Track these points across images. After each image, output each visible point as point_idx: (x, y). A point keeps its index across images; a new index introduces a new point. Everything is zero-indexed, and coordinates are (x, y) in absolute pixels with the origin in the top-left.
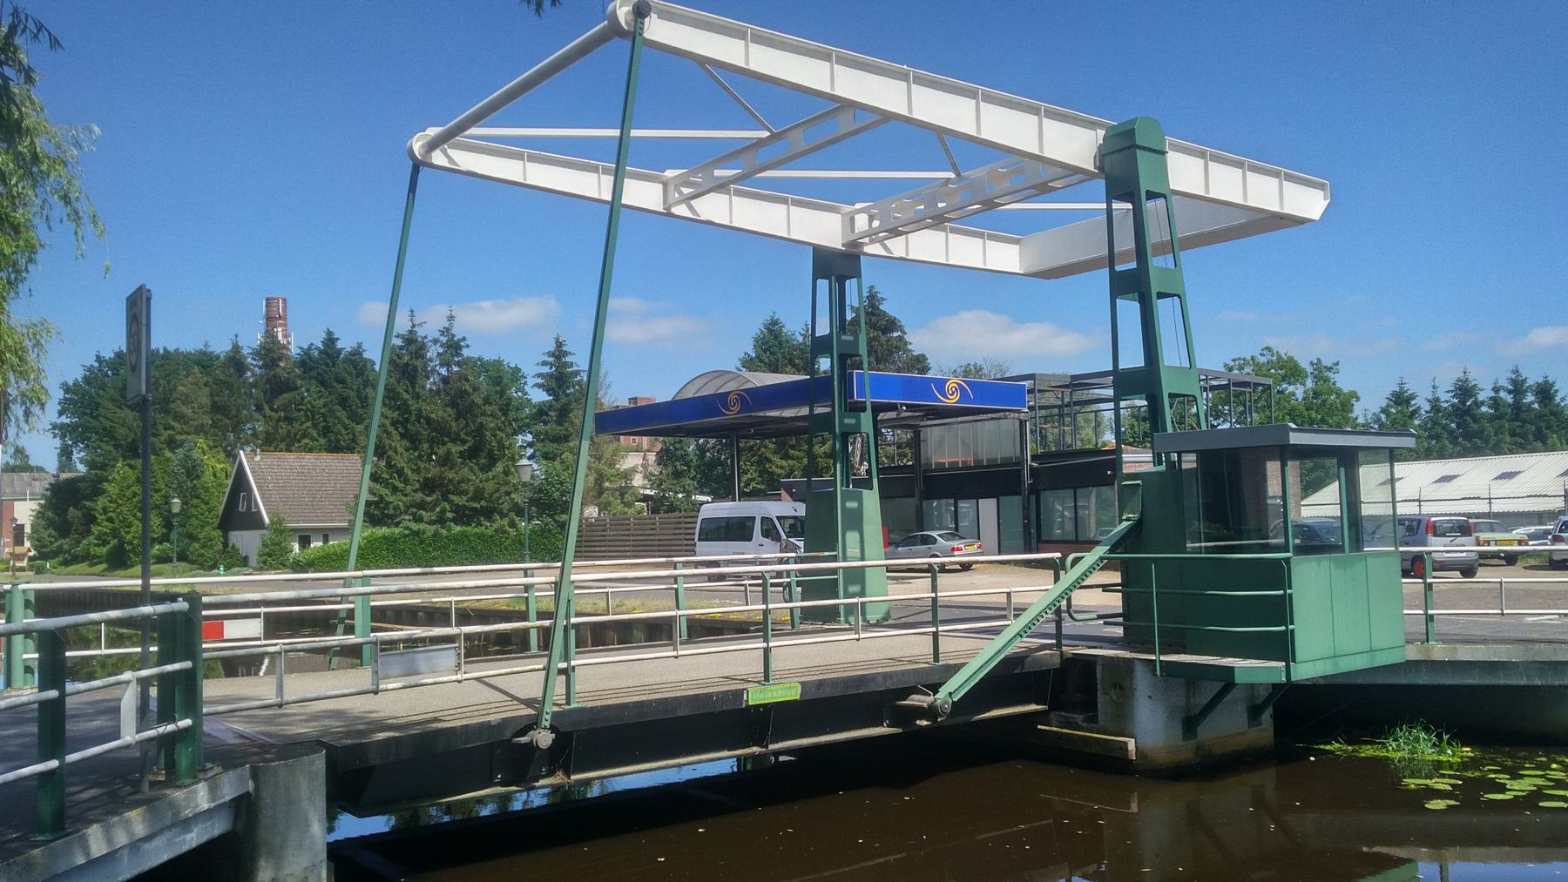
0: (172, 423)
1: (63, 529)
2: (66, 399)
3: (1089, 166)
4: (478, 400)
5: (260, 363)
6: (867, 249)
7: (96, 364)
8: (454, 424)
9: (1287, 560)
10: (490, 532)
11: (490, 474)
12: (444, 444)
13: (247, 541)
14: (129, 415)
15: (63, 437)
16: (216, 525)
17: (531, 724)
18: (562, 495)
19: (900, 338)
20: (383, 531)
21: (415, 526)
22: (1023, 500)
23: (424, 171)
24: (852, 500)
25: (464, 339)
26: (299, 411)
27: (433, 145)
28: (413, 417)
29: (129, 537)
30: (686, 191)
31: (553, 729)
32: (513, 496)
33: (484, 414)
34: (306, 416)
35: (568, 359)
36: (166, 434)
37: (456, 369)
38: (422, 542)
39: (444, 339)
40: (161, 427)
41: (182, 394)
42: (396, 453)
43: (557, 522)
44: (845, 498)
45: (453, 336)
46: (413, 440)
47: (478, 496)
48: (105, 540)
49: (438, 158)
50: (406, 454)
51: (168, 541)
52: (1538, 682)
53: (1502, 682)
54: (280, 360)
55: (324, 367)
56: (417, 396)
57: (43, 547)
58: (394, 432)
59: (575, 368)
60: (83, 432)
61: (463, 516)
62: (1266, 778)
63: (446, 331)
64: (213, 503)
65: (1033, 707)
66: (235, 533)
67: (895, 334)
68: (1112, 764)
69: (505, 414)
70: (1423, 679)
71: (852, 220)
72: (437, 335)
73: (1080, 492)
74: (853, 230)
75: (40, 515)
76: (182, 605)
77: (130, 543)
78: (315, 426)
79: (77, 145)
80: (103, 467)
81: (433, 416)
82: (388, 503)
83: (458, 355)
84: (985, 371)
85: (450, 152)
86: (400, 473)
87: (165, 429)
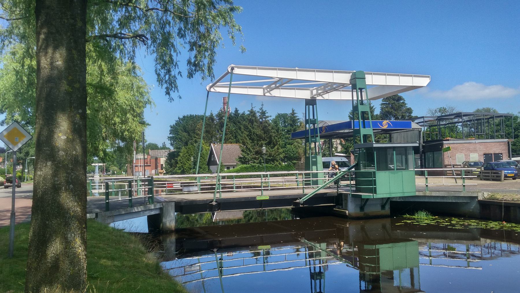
0: (196, 136)
1: (171, 165)
2: (171, 130)
3: (349, 83)
4: (270, 128)
5: (218, 118)
6: (317, 98)
7: (178, 120)
8: (263, 135)
9: (374, 172)
10: (274, 166)
11: (274, 149)
12: (261, 141)
13: (212, 168)
14: (185, 134)
15: (171, 140)
16: (206, 164)
17: (212, 201)
18: (294, 155)
19: (403, 103)
20: (245, 165)
21: (253, 164)
22: (420, 155)
23: (210, 93)
24: (314, 158)
25: (266, 111)
26: (228, 131)
27: (211, 87)
28: (252, 134)
29: (185, 167)
30: (268, 90)
31: (216, 202)
32: (280, 155)
33: (271, 132)
34: (230, 133)
35: (296, 115)
36: (194, 139)
37: (264, 119)
38: (255, 169)
39: (261, 111)
40: (193, 137)
41: (198, 128)
42: (248, 144)
43: (293, 163)
44: (313, 158)
45: (263, 110)
46: (252, 140)
47: (270, 156)
48: (180, 168)
49: (212, 90)
50: (251, 144)
51: (194, 169)
52: (454, 201)
53: (445, 201)
54: (223, 117)
55: (235, 119)
56: (253, 128)
57: (167, 170)
58: (248, 138)
59: (298, 118)
60: (176, 139)
61: (267, 161)
62: (387, 222)
63: (261, 109)
64: (206, 158)
65: (332, 204)
66: (211, 166)
67: (402, 101)
68: (344, 217)
69: (278, 132)
70: (426, 200)
71: (312, 92)
72: (259, 110)
73: (435, 153)
74: (312, 94)
75: (166, 162)
76: (150, 178)
77: (186, 169)
78: (232, 136)
79: (150, 89)
80: (180, 148)
81: (257, 133)
82: (246, 158)
83: (264, 115)
84: (447, 109)
85: (215, 88)
86: (249, 149)
87: (194, 138)
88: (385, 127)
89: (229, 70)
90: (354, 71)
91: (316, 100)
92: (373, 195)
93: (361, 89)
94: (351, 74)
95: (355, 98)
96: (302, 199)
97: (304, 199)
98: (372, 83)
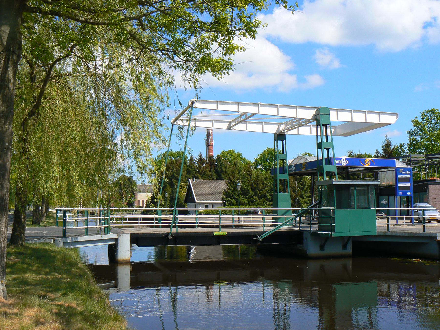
31: (172, 236)
70: (374, 240)
88: (367, 165)
89: (190, 104)
90: (319, 107)
91: (285, 135)
92: (331, 233)
93: (326, 125)
94: (316, 110)
97: (264, 236)
98: (366, 121)
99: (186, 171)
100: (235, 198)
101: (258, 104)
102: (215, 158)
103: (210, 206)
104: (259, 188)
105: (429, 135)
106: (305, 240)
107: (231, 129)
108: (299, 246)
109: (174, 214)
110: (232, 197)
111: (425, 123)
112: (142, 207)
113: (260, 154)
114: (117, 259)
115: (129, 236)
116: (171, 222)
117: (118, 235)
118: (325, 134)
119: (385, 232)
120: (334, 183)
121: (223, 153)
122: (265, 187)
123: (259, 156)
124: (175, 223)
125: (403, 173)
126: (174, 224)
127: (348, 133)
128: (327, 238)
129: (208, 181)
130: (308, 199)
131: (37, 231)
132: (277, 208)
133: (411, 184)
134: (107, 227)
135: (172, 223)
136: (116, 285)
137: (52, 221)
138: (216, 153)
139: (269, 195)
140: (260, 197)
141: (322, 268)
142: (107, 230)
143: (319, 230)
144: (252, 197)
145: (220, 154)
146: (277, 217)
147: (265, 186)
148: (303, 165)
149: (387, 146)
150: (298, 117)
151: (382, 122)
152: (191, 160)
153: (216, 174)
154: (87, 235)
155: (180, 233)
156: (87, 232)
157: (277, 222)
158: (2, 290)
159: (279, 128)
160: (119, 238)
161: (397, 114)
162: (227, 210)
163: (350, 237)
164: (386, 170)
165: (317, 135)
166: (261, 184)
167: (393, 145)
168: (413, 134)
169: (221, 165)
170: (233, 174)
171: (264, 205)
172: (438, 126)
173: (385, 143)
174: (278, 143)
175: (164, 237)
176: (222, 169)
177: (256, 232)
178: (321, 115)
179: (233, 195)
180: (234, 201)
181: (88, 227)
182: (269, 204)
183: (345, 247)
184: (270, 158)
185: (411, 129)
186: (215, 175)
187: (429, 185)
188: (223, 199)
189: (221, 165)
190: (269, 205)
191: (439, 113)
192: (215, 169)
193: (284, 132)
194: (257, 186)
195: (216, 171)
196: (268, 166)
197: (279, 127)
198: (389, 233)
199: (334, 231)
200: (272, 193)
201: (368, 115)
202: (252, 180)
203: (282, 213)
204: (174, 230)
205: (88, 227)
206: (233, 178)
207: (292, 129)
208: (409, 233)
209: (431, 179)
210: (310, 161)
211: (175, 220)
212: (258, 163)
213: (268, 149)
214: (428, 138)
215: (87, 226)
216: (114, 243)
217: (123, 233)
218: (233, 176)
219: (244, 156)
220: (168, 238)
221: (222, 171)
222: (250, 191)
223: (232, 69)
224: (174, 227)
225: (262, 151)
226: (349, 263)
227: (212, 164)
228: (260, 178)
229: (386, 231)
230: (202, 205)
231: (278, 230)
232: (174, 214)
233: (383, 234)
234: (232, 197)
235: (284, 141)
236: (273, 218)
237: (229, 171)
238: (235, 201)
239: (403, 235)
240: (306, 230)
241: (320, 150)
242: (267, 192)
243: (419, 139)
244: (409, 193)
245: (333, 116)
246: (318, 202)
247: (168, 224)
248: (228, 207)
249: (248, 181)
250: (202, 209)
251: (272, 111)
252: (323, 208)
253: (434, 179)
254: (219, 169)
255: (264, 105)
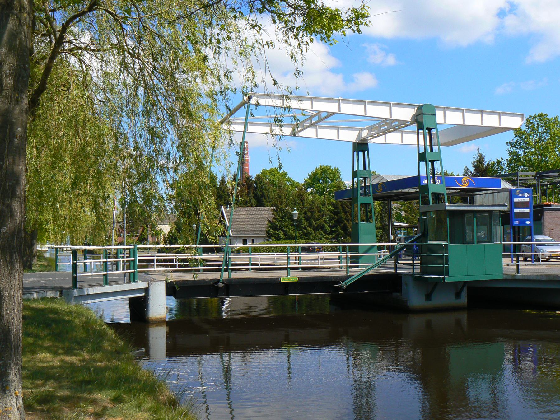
31: (223, 283)
88: (465, 186)
90: (421, 104)
91: (367, 144)
92: (444, 278)
93: (429, 129)
94: (416, 108)
95: (422, 142)
96: (345, 282)
97: (349, 282)
98: (482, 123)
99: (217, 196)
100: (283, 230)
101: (339, 100)
102: (253, 179)
103: (249, 241)
104: (315, 216)
105: (534, 148)
106: (404, 287)
107: (295, 136)
108: (395, 294)
109: (226, 252)
110: (279, 228)
111: (530, 131)
112: (158, 244)
113: (310, 174)
114: (148, 318)
115: (163, 284)
116: (222, 263)
117: (149, 283)
118: (428, 143)
119: (514, 275)
120: (448, 208)
121: (264, 172)
122: (322, 216)
123: (309, 175)
124: (227, 265)
125: (520, 195)
126: (225, 267)
127: (453, 141)
128: (436, 284)
129: (246, 208)
130: (379, 231)
131: (31, 280)
132: (358, 243)
133: (530, 210)
134: (134, 273)
135: (223, 265)
136: (147, 354)
137: (45, 263)
138: (254, 172)
139: (328, 225)
140: (316, 229)
141: (429, 324)
142: (133, 278)
143: (422, 272)
144: (305, 228)
145: (259, 173)
146: (358, 256)
147: (323, 215)
148: (379, 186)
149: (480, 162)
150: (393, 118)
151: (503, 125)
152: (223, 181)
153: (255, 199)
154: (107, 284)
155: (235, 279)
156: (106, 281)
157: (358, 263)
158: (16, 410)
159: (359, 135)
160: (151, 288)
161: (522, 115)
162: (274, 247)
163: (466, 283)
164: (485, 192)
165: (418, 145)
166: (317, 212)
167: (487, 161)
168: (515, 146)
169: (261, 188)
170: (280, 198)
171: (321, 239)
172: (546, 135)
173: (477, 158)
174: (358, 154)
175: (213, 285)
176: (263, 193)
177: (337, 277)
178: (424, 116)
179: (280, 226)
180: (282, 234)
181: (108, 273)
182: (328, 238)
183: (458, 295)
184: (324, 178)
185: (513, 140)
186: (253, 201)
187: (544, 212)
188: (267, 232)
189: (261, 188)
190: (327, 239)
191: (548, 118)
192: (253, 193)
193: (367, 140)
194: (312, 214)
195: (256, 196)
196: (321, 189)
197: (359, 133)
198: (519, 277)
199: (447, 274)
200: (332, 223)
201: (484, 116)
202: (305, 206)
203: (373, 249)
204: (225, 275)
205: (108, 273)
206: (281, 204)
207: (378, 136)
208: (547, 276)
209: (545, 203)
210: (389, 180)
211: (226, 261)
212: (308, 184)
213: (321, 166)
214: (533, 152)
215: (106, 271)
216: (143, 294)
217: (155, 280)
218: (280, 202)
219: (290, 176)
220: (218, 287)
221: (263, 195)
222: (303, 221)
223: (366, 23)
224: (226, 270)
225: (313, 170)
226: (464, 317)
227: (250, 187)
228: (316, 205)
229: (514, 273)
230: (238, 240)
231: (367, 273)
232: (226, 252)
233: (510, 278)
234: (279, 228)
235: (366, 152)
236: (352, 257)
237: (273, 195)
238: (284, 234)
239: (539, 278)
240: (405, 273)
241: (423, 164)
242: (325, 222)
243: (521, 153)
244: (528, 222)
245: (439, 116)
246: (420, 234)
247: (217, 267)
248: (275, 242)
249: (300, 207)
250: (239, 245)
251: (358, 109)
252: (430, 242)
253: (550, 203)
254: (259, 193)
255: (348, 101)
